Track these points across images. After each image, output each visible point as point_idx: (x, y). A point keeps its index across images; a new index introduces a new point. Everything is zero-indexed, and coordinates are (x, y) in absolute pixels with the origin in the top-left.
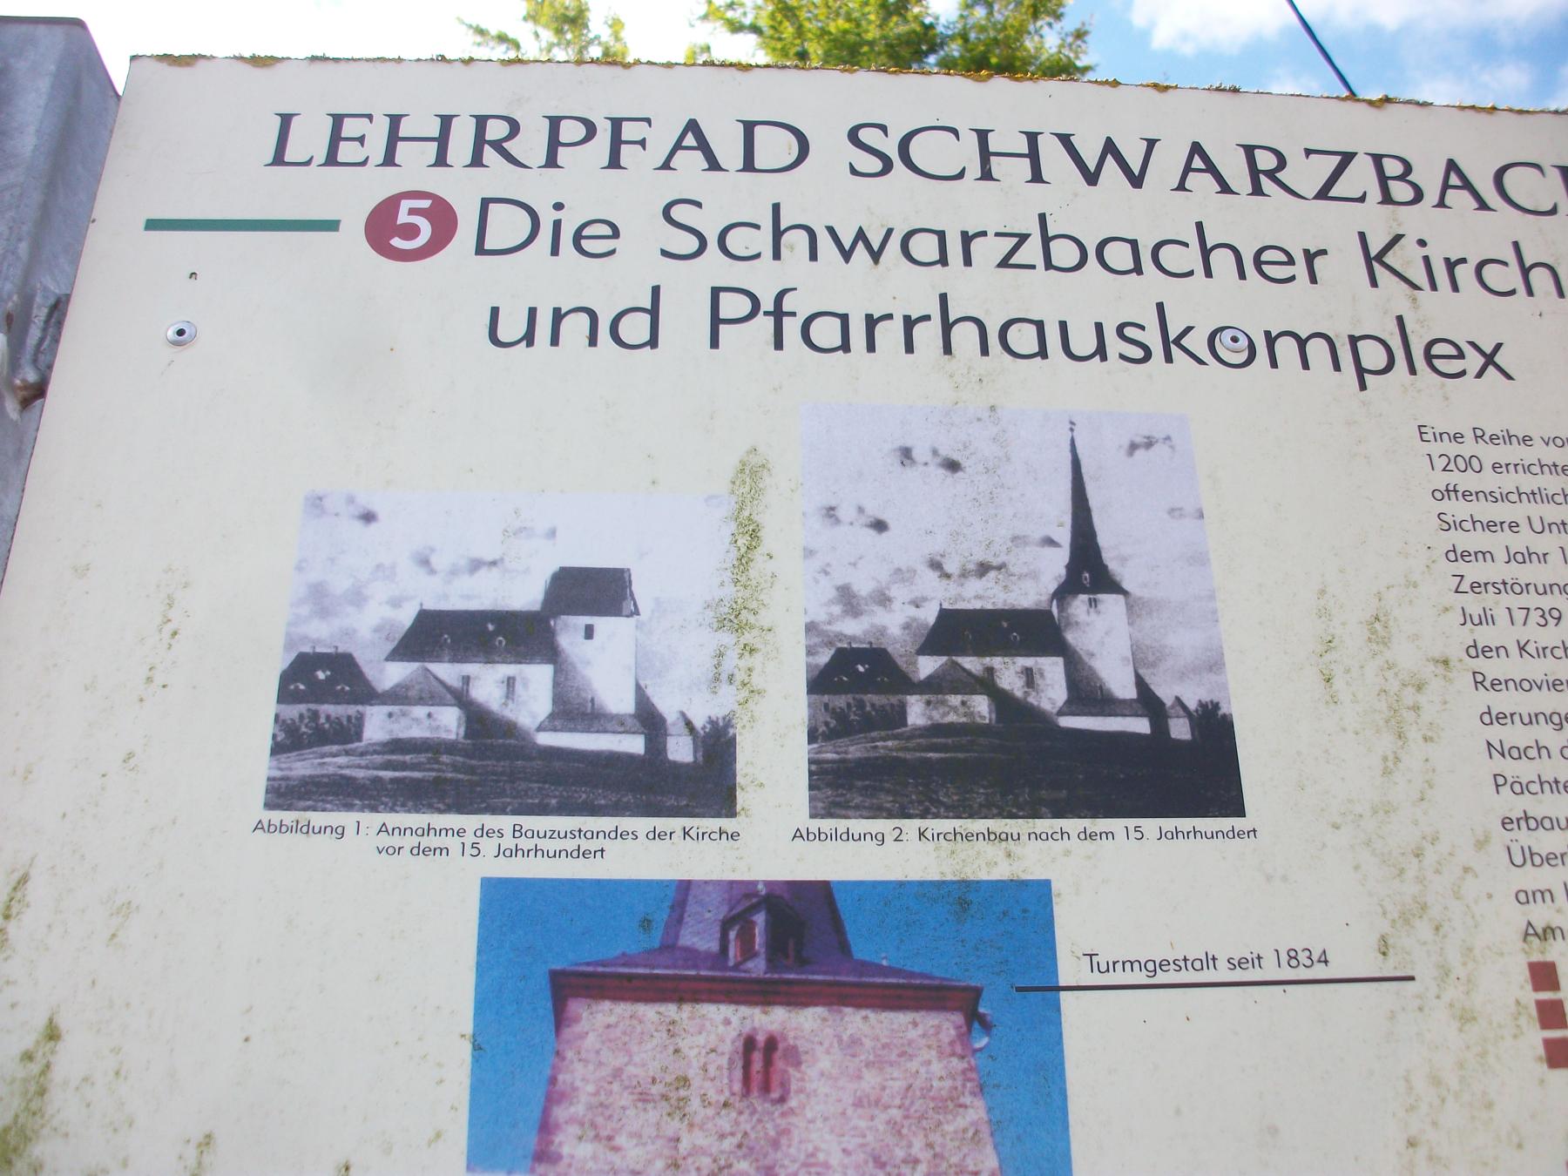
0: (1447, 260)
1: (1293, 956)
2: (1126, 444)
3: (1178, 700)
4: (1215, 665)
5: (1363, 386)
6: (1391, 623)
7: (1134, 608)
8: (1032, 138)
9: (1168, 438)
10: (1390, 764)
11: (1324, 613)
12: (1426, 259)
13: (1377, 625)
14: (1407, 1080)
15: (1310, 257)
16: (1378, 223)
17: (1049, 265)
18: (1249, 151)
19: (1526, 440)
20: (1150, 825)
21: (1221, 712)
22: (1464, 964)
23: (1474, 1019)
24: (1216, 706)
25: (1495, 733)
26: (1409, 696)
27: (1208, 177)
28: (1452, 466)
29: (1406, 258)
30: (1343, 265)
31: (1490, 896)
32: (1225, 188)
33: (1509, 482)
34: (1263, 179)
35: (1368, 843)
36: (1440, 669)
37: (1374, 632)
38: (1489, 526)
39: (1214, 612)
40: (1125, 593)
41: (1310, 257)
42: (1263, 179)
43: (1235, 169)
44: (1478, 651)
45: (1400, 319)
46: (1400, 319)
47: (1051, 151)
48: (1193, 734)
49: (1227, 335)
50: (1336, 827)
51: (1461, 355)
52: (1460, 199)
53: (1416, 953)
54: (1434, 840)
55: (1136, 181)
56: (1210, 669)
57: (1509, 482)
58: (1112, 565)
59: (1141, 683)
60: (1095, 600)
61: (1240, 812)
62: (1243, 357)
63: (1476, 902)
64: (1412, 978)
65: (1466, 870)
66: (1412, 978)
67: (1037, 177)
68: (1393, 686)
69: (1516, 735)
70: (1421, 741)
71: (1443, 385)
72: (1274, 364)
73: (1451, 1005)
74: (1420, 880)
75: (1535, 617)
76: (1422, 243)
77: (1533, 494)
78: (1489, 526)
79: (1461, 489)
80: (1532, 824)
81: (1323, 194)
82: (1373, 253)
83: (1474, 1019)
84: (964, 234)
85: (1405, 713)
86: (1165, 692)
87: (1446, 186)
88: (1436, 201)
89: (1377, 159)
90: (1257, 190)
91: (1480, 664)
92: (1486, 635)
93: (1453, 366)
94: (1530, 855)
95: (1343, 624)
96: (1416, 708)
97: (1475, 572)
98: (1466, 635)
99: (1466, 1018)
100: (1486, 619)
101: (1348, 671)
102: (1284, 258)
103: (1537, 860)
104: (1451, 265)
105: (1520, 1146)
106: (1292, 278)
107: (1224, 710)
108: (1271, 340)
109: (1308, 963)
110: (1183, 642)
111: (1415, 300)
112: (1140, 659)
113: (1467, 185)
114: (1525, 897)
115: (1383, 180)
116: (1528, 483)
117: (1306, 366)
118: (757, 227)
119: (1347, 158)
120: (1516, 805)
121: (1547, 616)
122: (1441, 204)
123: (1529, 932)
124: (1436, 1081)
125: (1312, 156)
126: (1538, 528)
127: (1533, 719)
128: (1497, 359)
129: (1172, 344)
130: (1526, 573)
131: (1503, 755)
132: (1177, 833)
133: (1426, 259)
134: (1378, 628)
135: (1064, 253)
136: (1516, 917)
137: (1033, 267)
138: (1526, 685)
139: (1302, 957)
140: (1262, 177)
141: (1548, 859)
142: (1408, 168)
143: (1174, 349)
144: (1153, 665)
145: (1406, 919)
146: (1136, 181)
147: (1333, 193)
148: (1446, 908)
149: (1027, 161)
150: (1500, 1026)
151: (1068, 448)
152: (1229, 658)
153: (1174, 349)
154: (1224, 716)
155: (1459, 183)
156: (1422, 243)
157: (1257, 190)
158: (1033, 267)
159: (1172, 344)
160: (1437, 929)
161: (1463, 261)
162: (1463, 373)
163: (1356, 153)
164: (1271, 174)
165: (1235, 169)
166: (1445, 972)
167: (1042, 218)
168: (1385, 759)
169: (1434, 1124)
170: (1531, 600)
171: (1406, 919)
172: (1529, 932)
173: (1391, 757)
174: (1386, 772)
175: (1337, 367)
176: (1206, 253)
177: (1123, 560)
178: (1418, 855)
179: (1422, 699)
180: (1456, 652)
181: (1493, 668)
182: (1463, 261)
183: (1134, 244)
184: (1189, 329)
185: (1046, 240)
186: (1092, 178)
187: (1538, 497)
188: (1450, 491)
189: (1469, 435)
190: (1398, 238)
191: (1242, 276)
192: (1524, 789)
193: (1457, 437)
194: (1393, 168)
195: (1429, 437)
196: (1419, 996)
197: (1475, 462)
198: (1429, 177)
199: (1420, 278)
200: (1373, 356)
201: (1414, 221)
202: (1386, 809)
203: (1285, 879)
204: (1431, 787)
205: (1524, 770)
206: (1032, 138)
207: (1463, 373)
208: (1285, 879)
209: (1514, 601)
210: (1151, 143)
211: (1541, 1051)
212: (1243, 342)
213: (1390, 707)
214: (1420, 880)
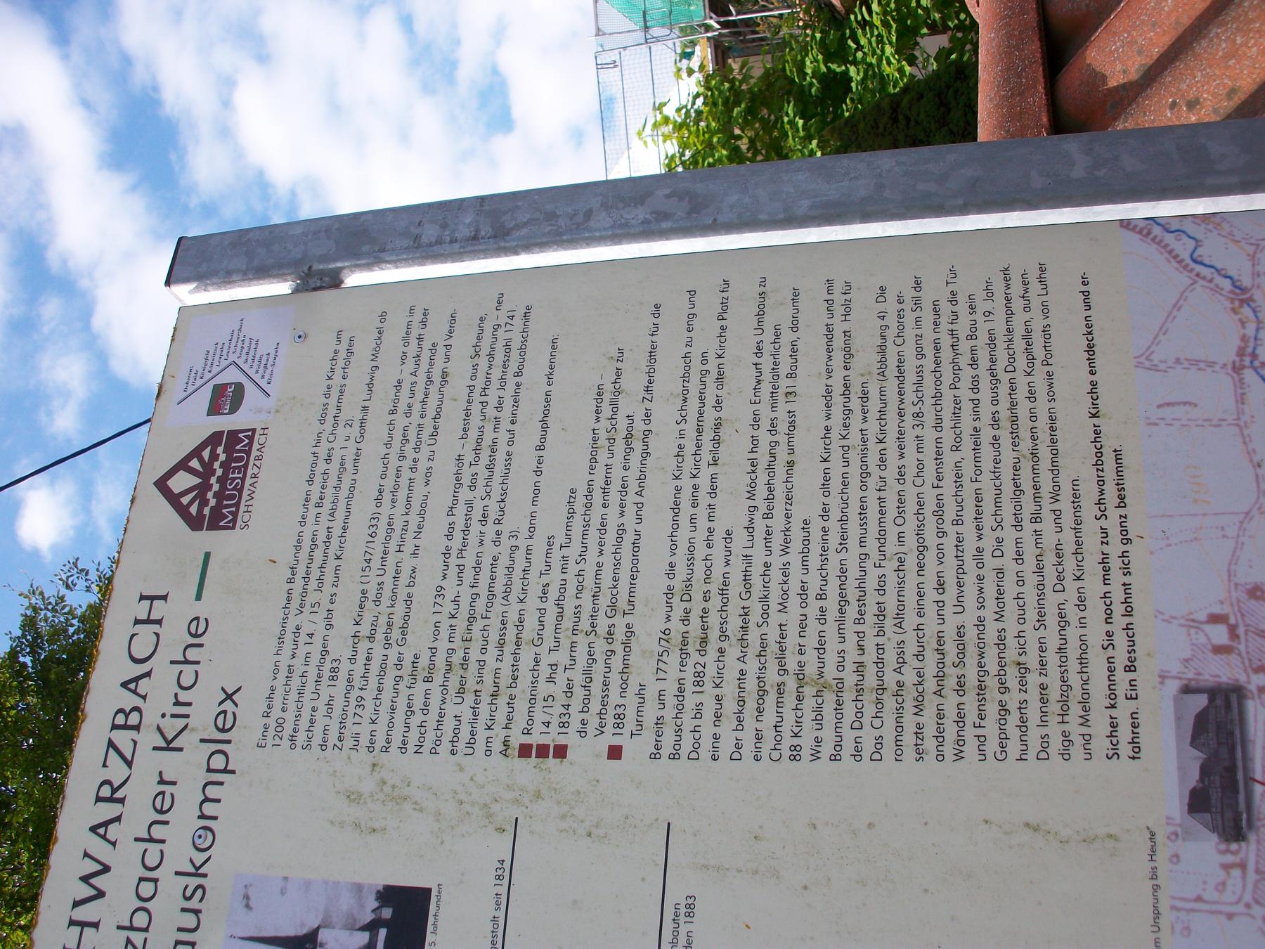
0: (174, 704)
1: (498, 877)
2: (245, 910)
3: (373, 911)
4: (359, 888)
5: (233, 772)
6: (352, 790)
7: (326, 924)
8: (72, 923)
9: (246, 886)
10: (417, 807)
11: (342, 825)
12: (173, 716)
13: (351, 797)
14: (562, 831)
15: (162, 782)
16: (148, 738)
17: (146, 930)
18: (99, 799)
19: (273, 689)
20: (429, 938)
21: (382, 890)
22: (514, 790)
23: (539, 791)
24: (378, 892)
25: (411, 747)
26: (387, 789)
27: (110, 827)
28: (280, 734)
29: (171, 726)
30: (170, 763)
31: (485, 770)
32: (118, 819)
33: (292, 706)
34: (117, 795)
35: (452, 828)
36: (377, 769)
37: (354, 800)
38: (312, 722)
39: (334, 883)
40: (318, 928)
41: (162, 782)
42: (117, 795)
43: (109, 811)
44: (371, 748)
45: (202, 741)
46: (202, 741)
47: (82, 913)
48: (389, 907)
49: (198, 841)
50: (442, 842)
51: (225, 712)
52: (143, 687)
53: (505, 813)
54: (456, 793)
55: (106, 869)
56: (361, 891)
57: (292, 706)
58: (304, 931)
59: (363, 929)
60: (320, 943)
61: (429, 890)
62: (209, 834)
63: (487, 777)
64: (517, 819)
65: (472, 779)
66: (517, 819)
67: (96, 925)
68: (381, 796)
69: (413, 736)
70: (409, 789)
71: (238, 727)
72: (215, 818)
73: (531, 801)
74: (473, 805)
75: (359, 711)
76: (163, 716)
77: (299, 693)
78: (312, 722)
79: (292, 733)
80: (455, 739)
81: (129, 764)
82: (164, 745)
83: (539, 791)
84: (175, 704)
85: (396, 794)
86: (368, 917)
87: (135, 692)
88: (142, 700)
89: (114, 727)
90: (122, 801)
91: (378, 746)
92: (364, 741)
93: (230, 717)
94: (470, 744)
95: (348, 815)
96: (393, 787)
97: (333, 738)
98: (363, 750)
99: (538, 795)
100: (356, 737)
101: (371, 819)
102: (195, 622)
103: (472, 741)
104: (177, 703)
105: (598, 781)
106: (172, 795)
107: (381, 888)
108: (202, 816)
109: (502, 870)
110: (346, 902)
111: (193, 729)
112: (351, 927)
113: (136, 679)
114: (488, 753)
115: (125, 727)
116: (294, 695)
117: (218, 801)
118: (181, 672)
119: (111, 744)
120: (446, 746)
121: (359, 704)
122: (144, 697)
123: (504, 753)
124: (563, 817)
125: (108, 763)
126: (382, 572)
127: (407, 725)
128: (229, 701)
129: (418, 356)
130: (337, 712)
131: (422, 746)
132: (435, 925)
133: (173, 716)
134: (353, 797)
135: (140, 920)
136: (497, 758)
137: (146, 939)
138: (391, 725)
139: (499, 872)
140: (115, 796)
141: (473, 734)
142: (121, 711)
143: (201, 871)
144: (355, 920)
145: (489, 816)
146: (106, 869)
147: (129, 757)
148: (488, 794)
149: (85, 929)
150: (544, 779)
151: (247, 943)
152: (358, 880)
153: (201, 871)
154: (384, 889)
155: (134, 684)
156: (163, 716)
157: (122, 801)
158: (146, 939)
159: (418, 356)
160: (496, 801)
161: (176, 695)
162: (234, 714)
163: (109, 738)
164: (114, 791)
165: (109, 811)
166: (516, 801)
167: (119, 928)
168: (415, 809)
169: (582, 821)
170: (351, 710)
171: (489, 816)
172: (504, 753)
173: (414, 806)
174: (421, 810)
175: (221, 784)
176: (187, 662)
177: (303, 925)
178: (461, 803)
179: (390, 782)
180: (370, 758)
181: (380, 742)
182: (176, 695)
183: (141, 879)
184: (191, 861)
185: (131, 928)
186: (101, 894)
187: (302, 692)
188: (292, 739)
189: (266, 720)
190: (158, 728)
191: (166, 823)
192: (439, 740)
193: (266, 727)
194: (120, 720)
195: (264, 742)
196: (525, 817)
197: (279, 721)
198: (129, 701)
199: (182, 722)
200: (218, 762)
201: (151, 717)
202: (438, 815)
203: (463, 874)
204: (431, 788)
205: (431, 736)
206: (72, 923)
207: (234, 714)
208: (463, 874)
209: (350, 720)
210: (86, 855)
211: (558, 760)
212: (201, 832)
213: (391, 800)
214: (473, 805)
